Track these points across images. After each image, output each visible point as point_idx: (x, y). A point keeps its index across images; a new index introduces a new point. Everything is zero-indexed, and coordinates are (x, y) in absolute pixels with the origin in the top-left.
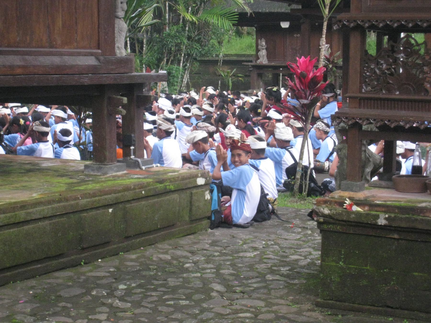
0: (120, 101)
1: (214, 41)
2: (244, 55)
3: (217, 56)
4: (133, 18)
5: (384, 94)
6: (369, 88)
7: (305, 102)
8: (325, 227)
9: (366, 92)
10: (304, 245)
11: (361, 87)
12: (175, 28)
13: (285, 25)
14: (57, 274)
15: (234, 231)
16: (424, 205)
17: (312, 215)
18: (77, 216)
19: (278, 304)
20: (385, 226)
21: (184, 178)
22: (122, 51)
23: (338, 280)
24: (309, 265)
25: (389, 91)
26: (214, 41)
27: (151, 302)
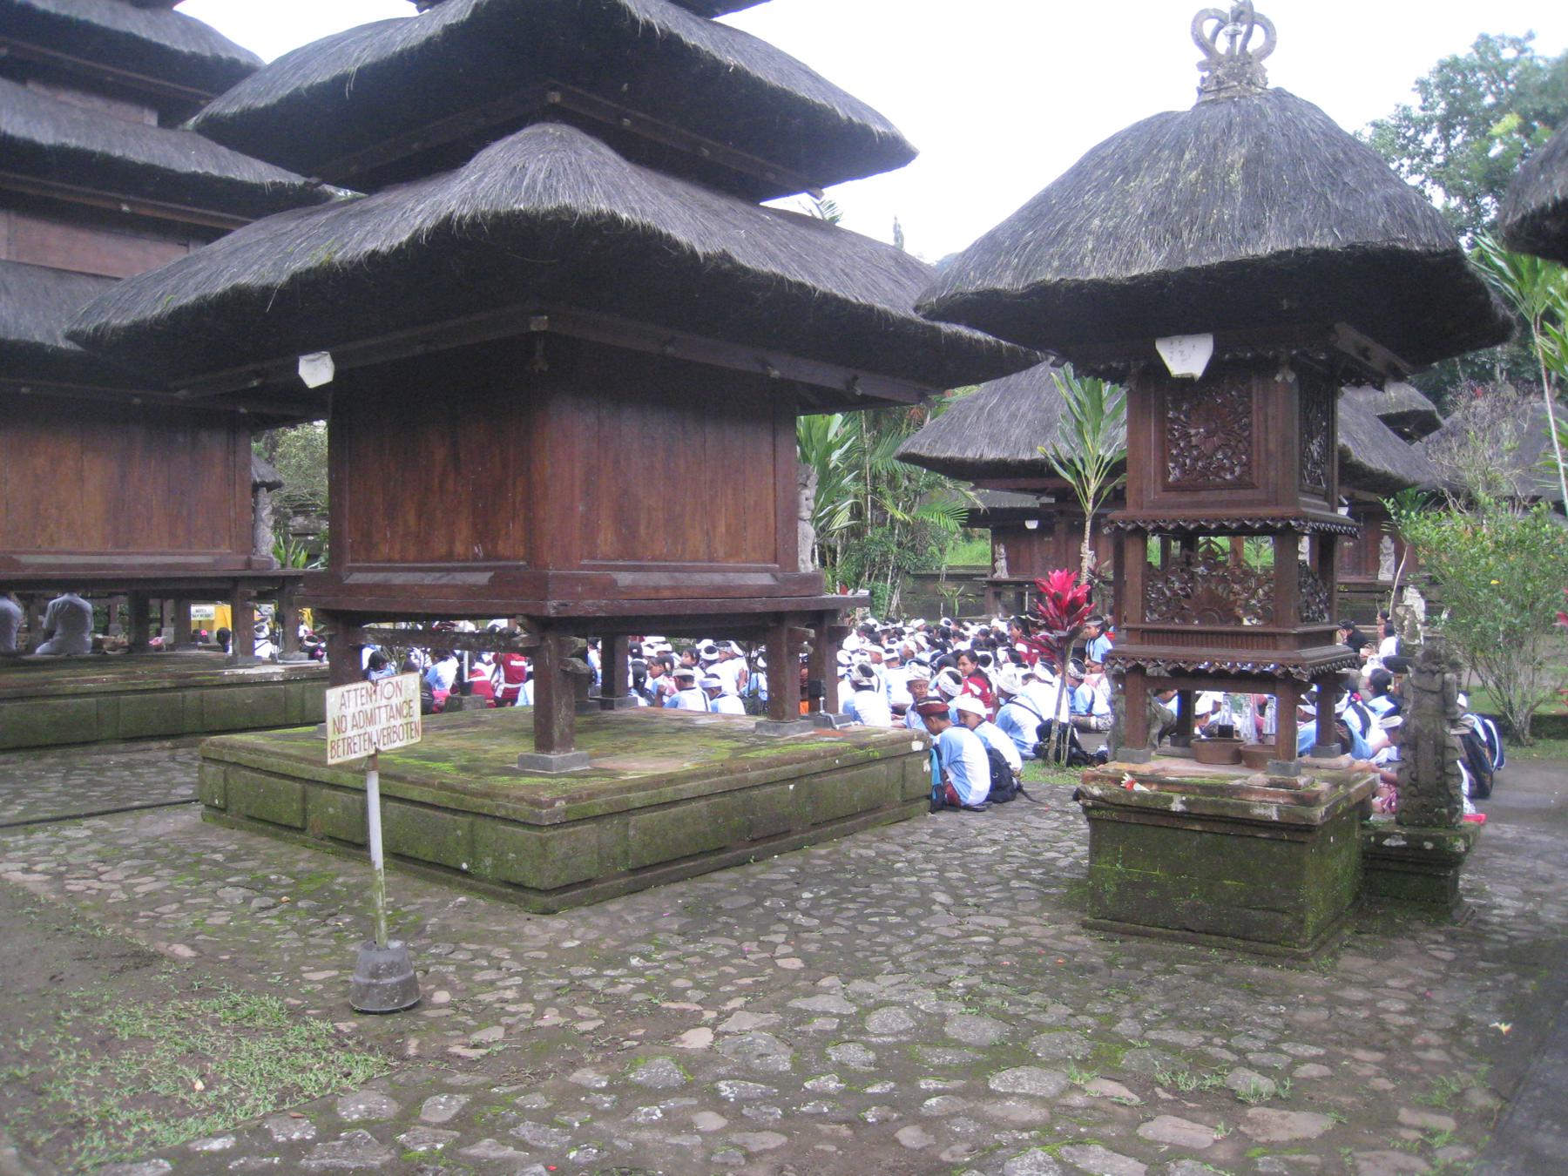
0: (804, 637)
1: (934, 549)
2: (975, 567)
3: (939, 568)
4: (821, 519)
5: (1177, 624)
6: (1156, 616)
7: (1063, 634)
8: (1095, 813)
9: (1152, 621)
10: (1065, 839)
11: (1144, 616)
12: (880, 531)
13: (1032, 525)
14: (716, 875)
15: (964, 816)
16: (1237, 782)
17: (1077, 796)
18: (744, 795)
19: (1027, 924)
20: (1182, 812)
21: (894, 742)
22: (807, 564)
23: (1114, 889)
24: (1071, 867)
25: (1185, 619)
26: (934, 549)
27: (848, 919)
